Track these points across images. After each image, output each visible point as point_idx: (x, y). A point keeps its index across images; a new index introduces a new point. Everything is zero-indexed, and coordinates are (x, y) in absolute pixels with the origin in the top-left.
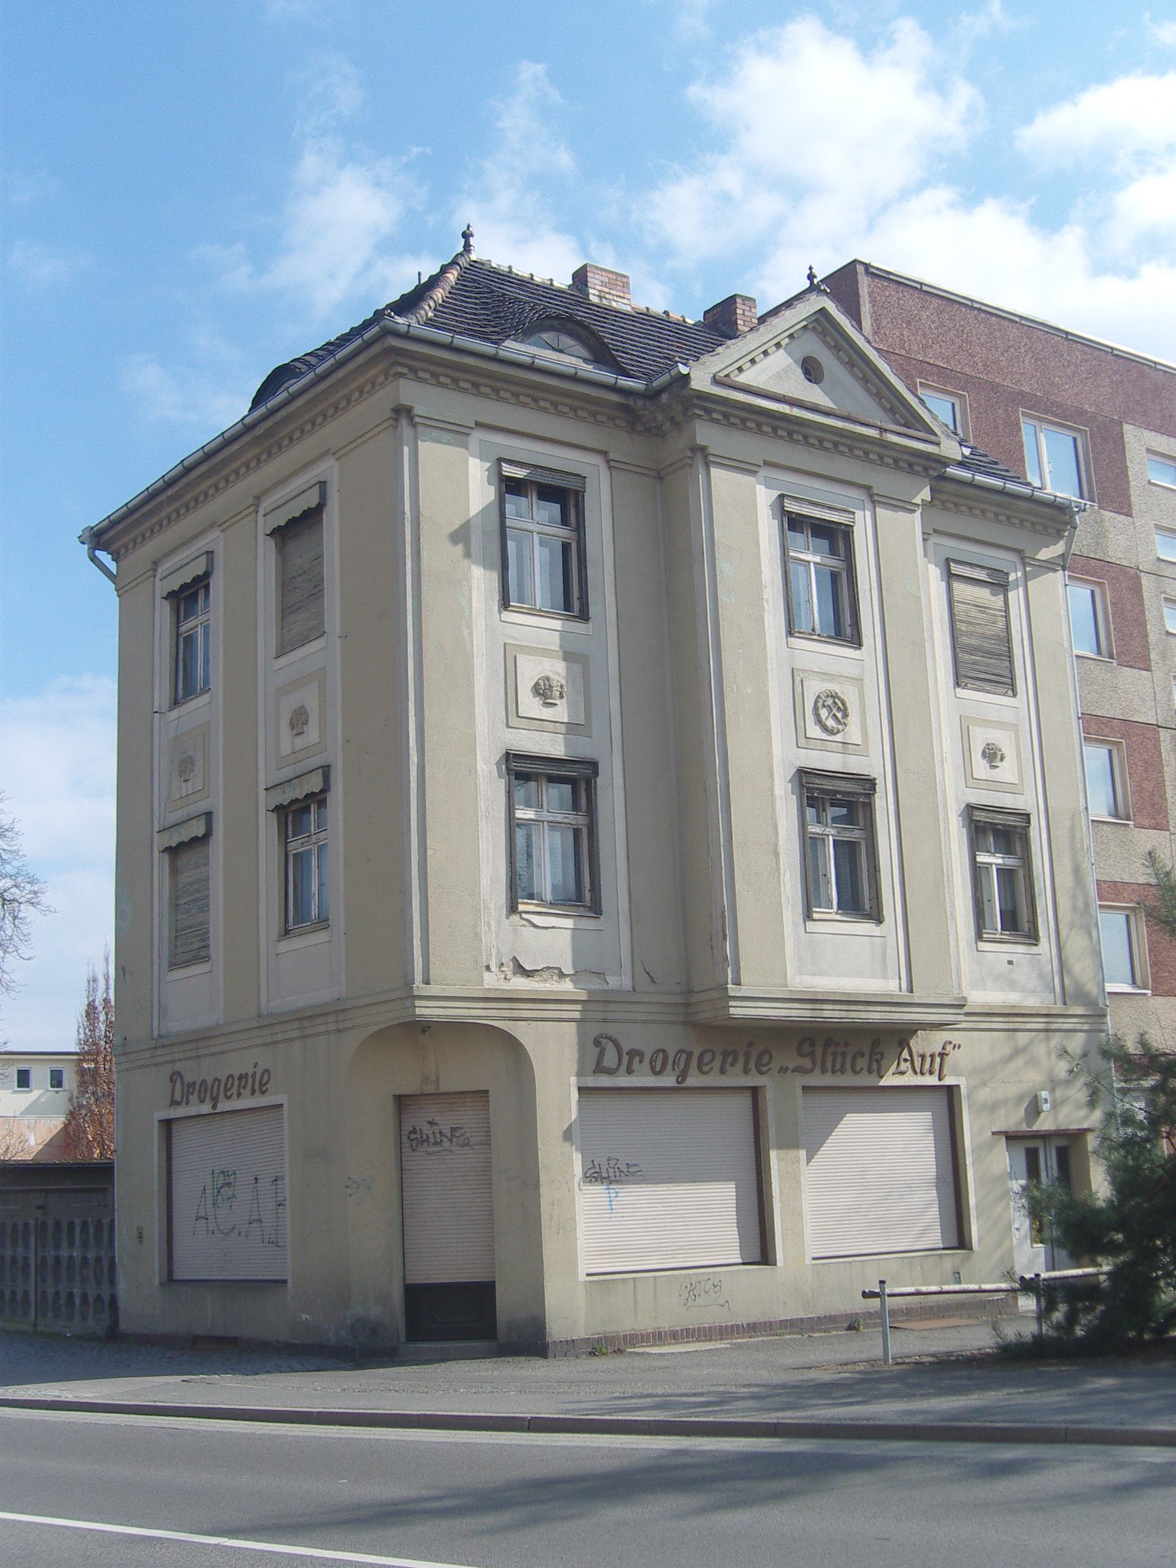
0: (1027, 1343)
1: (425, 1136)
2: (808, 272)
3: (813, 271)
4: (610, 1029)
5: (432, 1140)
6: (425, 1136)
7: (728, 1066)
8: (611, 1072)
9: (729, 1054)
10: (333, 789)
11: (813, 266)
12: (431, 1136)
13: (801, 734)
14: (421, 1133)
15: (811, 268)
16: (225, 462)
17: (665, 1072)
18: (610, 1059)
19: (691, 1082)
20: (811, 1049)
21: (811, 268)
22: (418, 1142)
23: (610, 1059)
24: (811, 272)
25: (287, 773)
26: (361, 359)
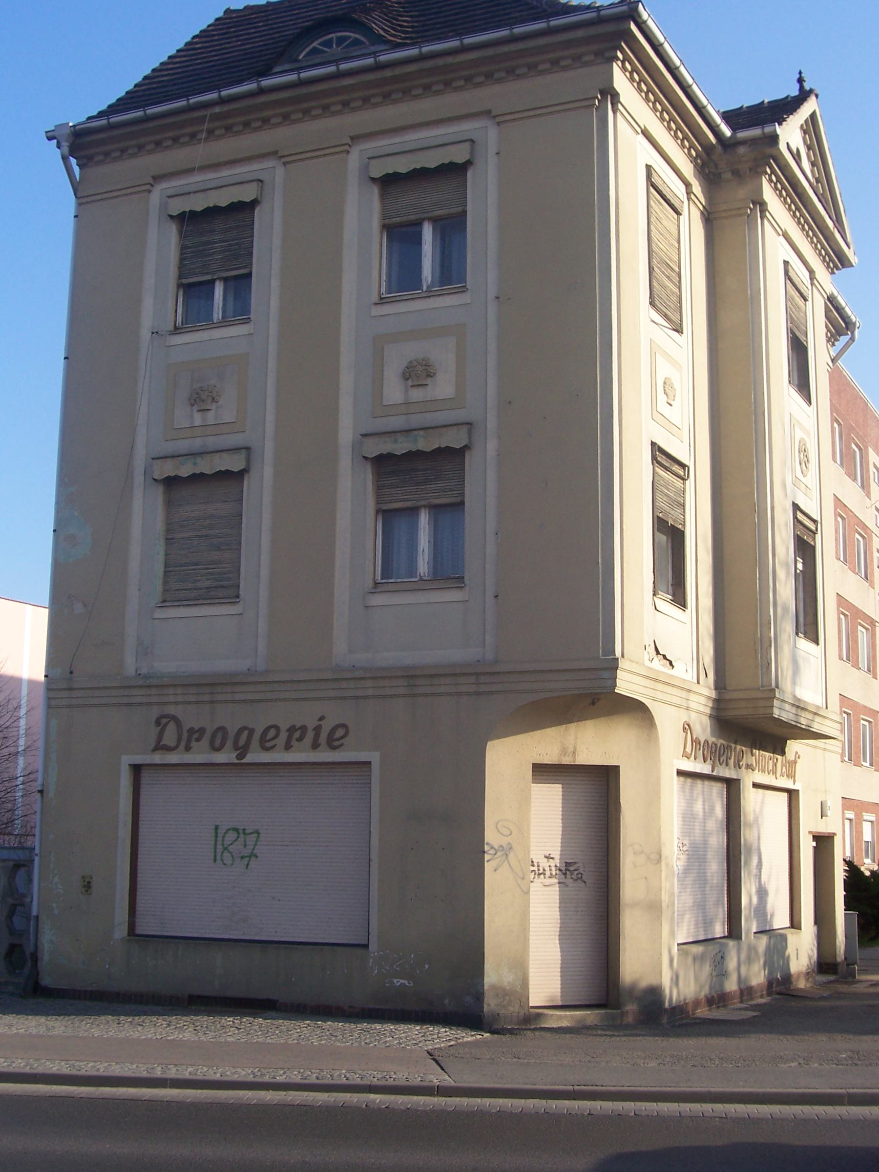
0: (762, 984)
1: (541, 869)
2: (798, 76)
3: (803, 75)
4: (171, 710)
5: (548, 873)
6: (541, 869)
7: (294, 743)
8: (169, 749)
9: (296, 730)
10: (254, 473)
11: (802, 71)
12: (547, 869)
13: (794, 475)
14: (538, 866)
15: (800, 73)
16: (325, 94)
17: (223, 750)
18: (169, 737)
19: (249, 758)
20: (321, 723)
21: (800, 73)
22: (535, 874)
23: (169, 737)
24: (801, 77)
25: (183, 446)
26: (580, 33)
